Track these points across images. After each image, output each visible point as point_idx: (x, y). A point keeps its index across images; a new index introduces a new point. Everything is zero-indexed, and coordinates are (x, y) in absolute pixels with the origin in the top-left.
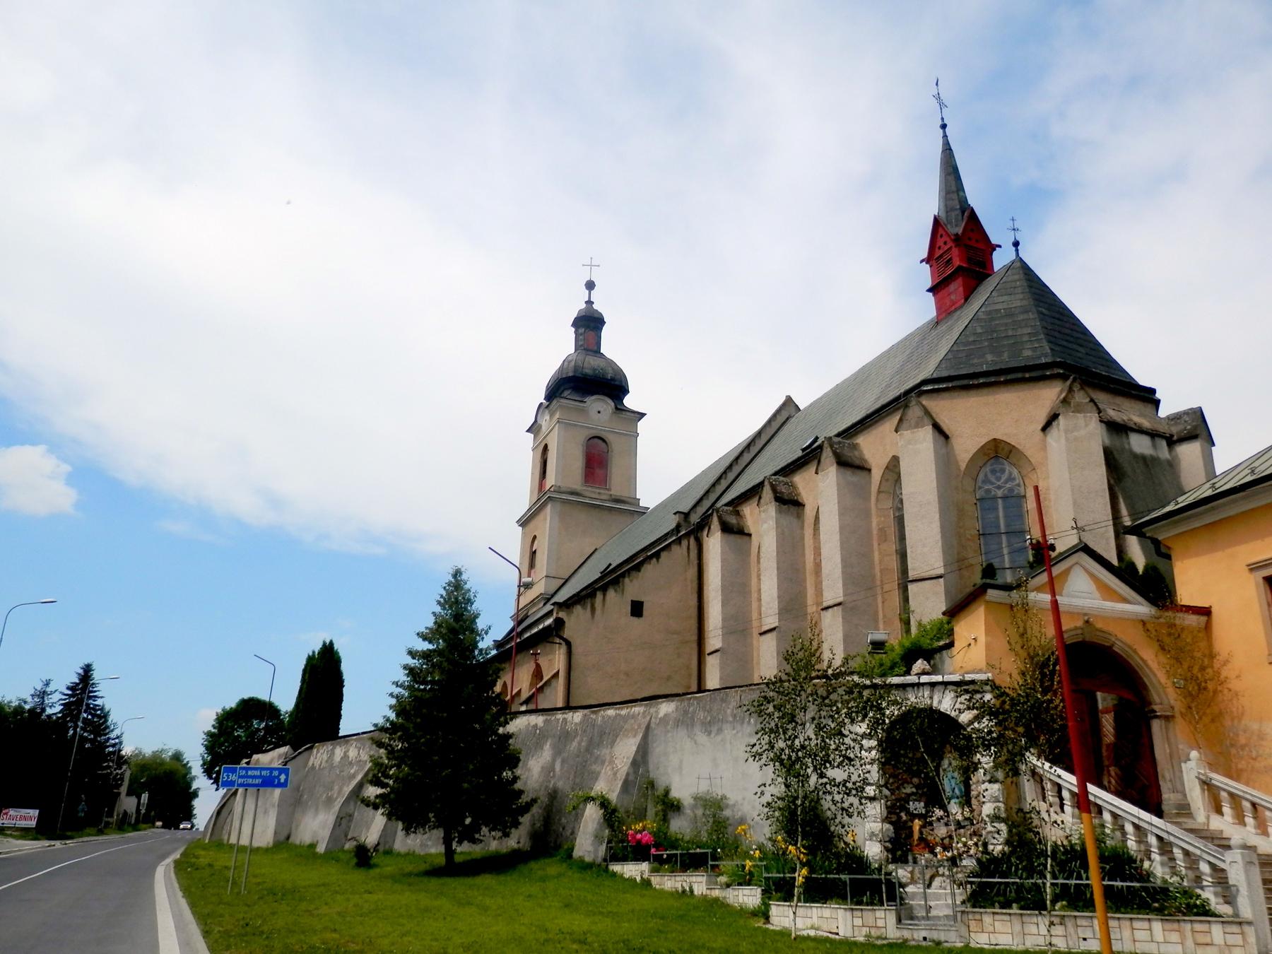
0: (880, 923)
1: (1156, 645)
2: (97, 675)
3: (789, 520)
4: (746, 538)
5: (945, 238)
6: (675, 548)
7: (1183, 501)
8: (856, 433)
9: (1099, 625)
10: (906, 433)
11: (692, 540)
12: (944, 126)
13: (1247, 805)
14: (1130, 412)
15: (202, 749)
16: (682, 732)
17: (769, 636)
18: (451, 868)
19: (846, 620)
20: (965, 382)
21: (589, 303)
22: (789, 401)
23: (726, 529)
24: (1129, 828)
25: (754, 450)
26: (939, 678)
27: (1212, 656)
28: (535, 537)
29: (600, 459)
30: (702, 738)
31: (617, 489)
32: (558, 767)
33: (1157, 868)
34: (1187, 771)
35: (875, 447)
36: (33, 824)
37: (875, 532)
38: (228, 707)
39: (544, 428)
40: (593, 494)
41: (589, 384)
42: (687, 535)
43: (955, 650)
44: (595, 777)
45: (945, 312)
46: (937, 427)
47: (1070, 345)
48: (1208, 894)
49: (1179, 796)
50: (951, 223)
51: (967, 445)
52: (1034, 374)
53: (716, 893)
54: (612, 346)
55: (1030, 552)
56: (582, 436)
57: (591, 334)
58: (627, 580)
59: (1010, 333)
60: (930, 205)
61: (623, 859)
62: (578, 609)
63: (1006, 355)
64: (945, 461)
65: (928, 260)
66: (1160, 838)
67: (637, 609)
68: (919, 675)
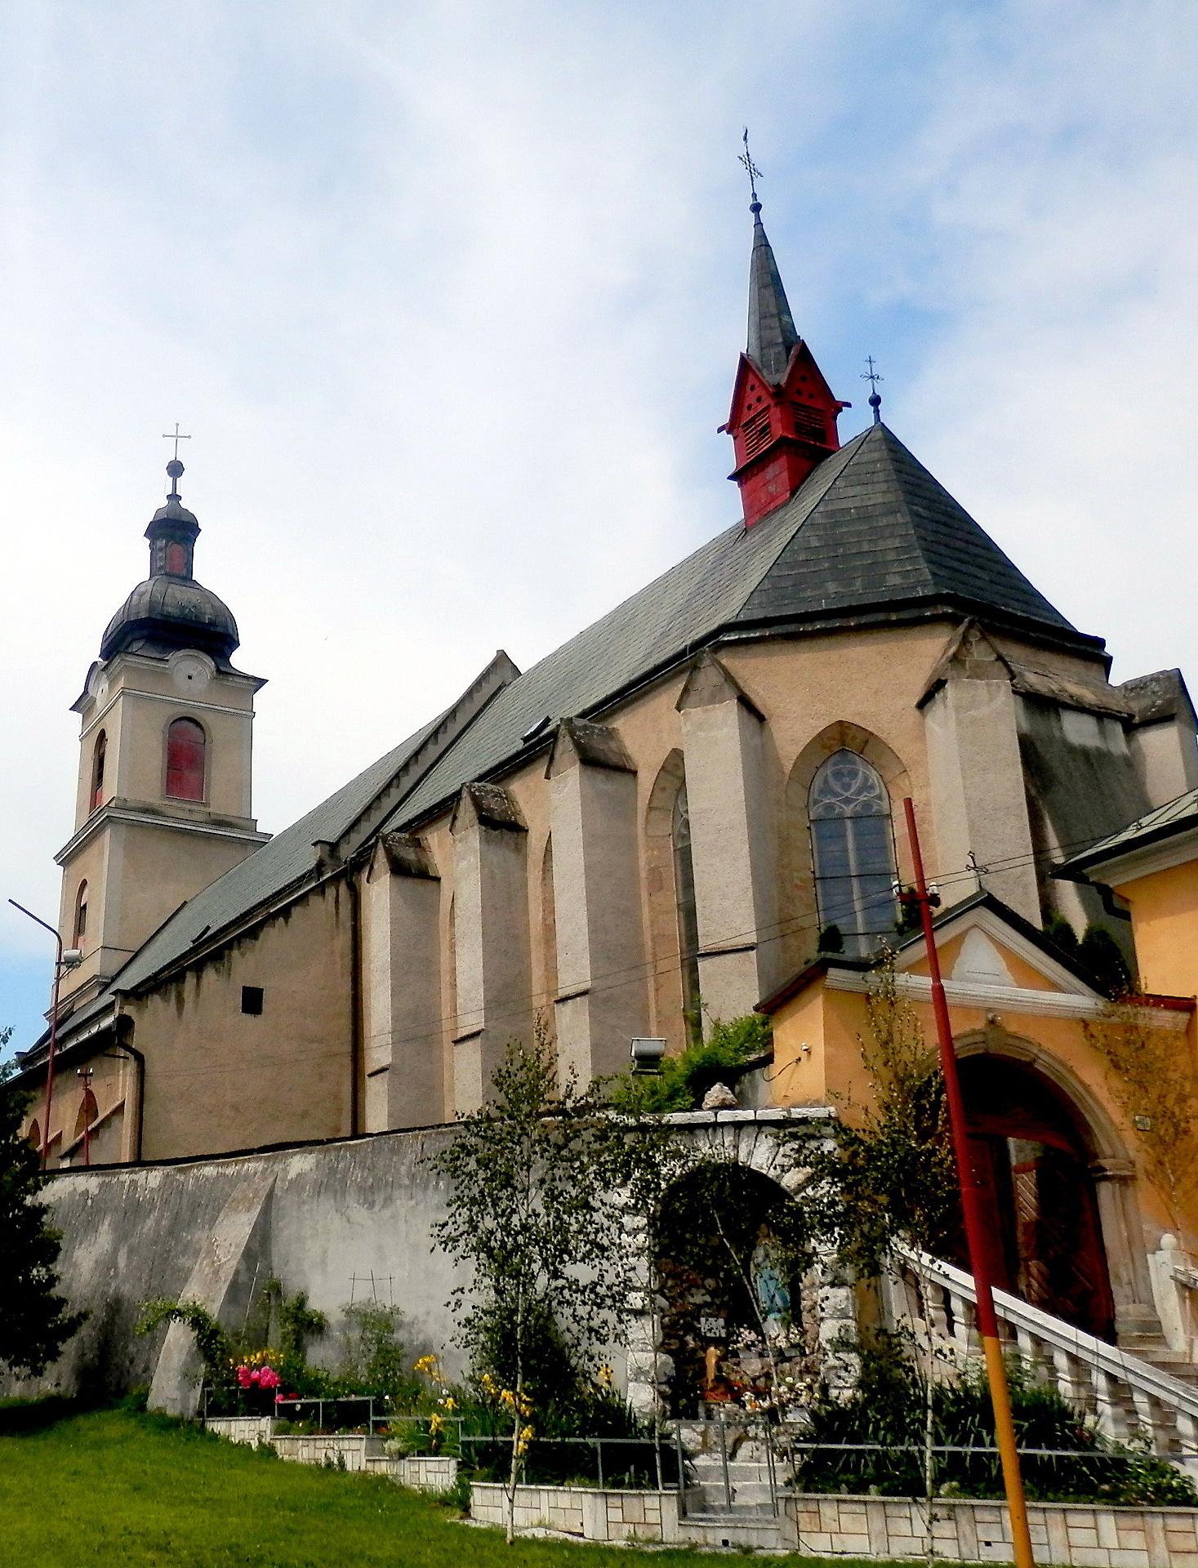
0: (653, 1517)
3: (502, 855)
4: (432, 885)
5: (759, 391)
6: (315, 900)
7: (1151, 823)
8: (613, 713)
9: (1012, 1028)
10: (695, 713)
11: (343, 887)
12: (756, 208)
14: (1062, 678)
16: (326, 1204)
17: (469, 1044)
20: (791, 628)
21: (174, 497)
24: (1061, 1361)
25: (444, 740)
26: (747, 1115)
28: (84, 883)
30: (359, 1213)
31: (219, 803)
32: (122, 1262)
35: (642, 735)
37: (643, 874)
39: (98, 703)
40: (179, 812)
42: (335, 879)
43: (774, 1068)
45: (758, 513)
46: (745, 702)
47: (964, 568)
49: (1144, 1308)
51: (795, 730)
52: (905, 615)
53: (382, 1468)
54: (212, 568)
58: (235, 953)
59: (866, 547)
60: (732, 336)
61: (231, 1412)
65: (730, 428)
66: (1111, 1378)
67: (252, 1001)
68: (716, 1109)
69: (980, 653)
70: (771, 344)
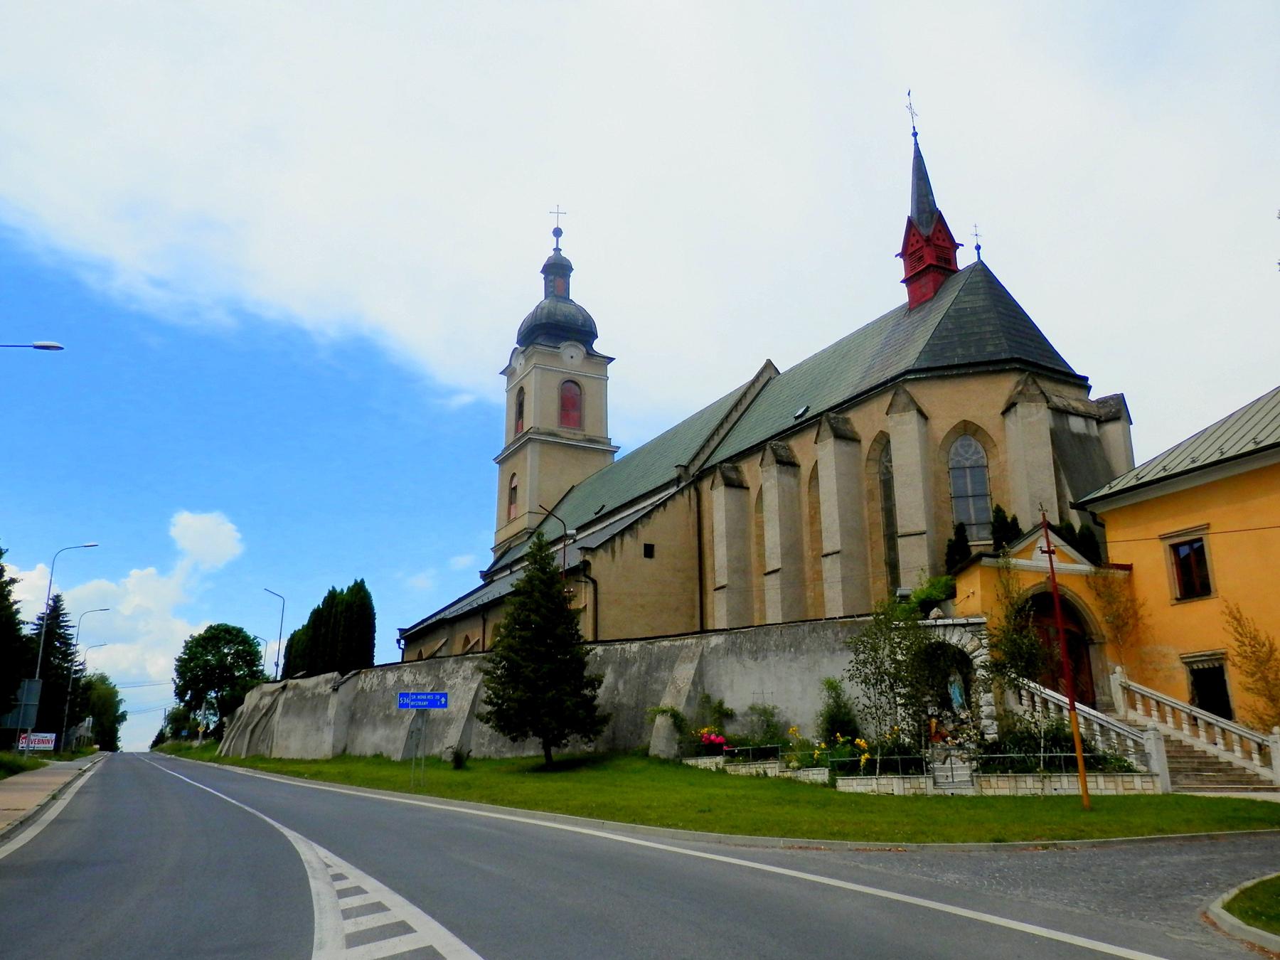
0: (923, 786)
1: (1094, 593)
2: (67, 606)
3: (789, 480)
4: (745, 491)
5: (917, 237)
6: (678, 497)
7: (1118, 485)
8: (848, 409)
10: (896, 416)
11: (692, 490)
12: (915, 134)
13: (1153, 703)
14: (1066, 396)
15: (174, 675)
16: (732, 659)
17: (773, 576)
18: (549, 767)
19: (844, 566)
20: (940, 373)
21: (557, 250)
22: (769, 364)
23: (729, 484)
24: (1096, 727)
25: (741, 408)
26: (950, 621)
27: (1133, 600)
29: (575, 403)
30: (750, 663)
31: (590, 430)
32: (621, 686)
33: (1100, 746)
34: (1116, 679)
35: (865, 422)
36: (51, 746)
38: (196, 634)
40: (568, 434)
41: (558, 330)
43: (957, 600)
44: (658, 695)
45: (917, 301)
46: (921, 412)
48: (1132, 760)
50: (921, 224)
51: (942, 424)
52: (997, 368)
53: (788, 774)
54: (581, 292)
55: (991, 514)
56: (555, 382)
57: (560, 281)
60: (904, 208)
61: (698, 754)
62: (601, 552)
63: (973, 350)
64: (926, 438)
65: (902, 255)
66: (1101, 726)
67: (649, 551)
68: (935, 619)
69: (1033, 390)
70: (924, 211)
